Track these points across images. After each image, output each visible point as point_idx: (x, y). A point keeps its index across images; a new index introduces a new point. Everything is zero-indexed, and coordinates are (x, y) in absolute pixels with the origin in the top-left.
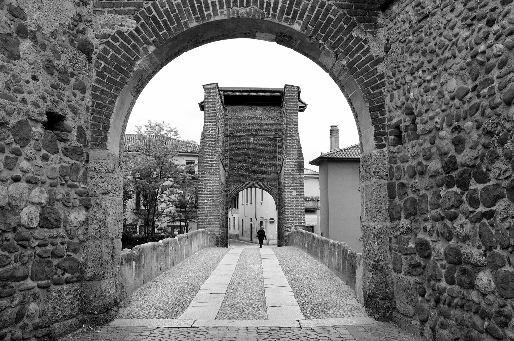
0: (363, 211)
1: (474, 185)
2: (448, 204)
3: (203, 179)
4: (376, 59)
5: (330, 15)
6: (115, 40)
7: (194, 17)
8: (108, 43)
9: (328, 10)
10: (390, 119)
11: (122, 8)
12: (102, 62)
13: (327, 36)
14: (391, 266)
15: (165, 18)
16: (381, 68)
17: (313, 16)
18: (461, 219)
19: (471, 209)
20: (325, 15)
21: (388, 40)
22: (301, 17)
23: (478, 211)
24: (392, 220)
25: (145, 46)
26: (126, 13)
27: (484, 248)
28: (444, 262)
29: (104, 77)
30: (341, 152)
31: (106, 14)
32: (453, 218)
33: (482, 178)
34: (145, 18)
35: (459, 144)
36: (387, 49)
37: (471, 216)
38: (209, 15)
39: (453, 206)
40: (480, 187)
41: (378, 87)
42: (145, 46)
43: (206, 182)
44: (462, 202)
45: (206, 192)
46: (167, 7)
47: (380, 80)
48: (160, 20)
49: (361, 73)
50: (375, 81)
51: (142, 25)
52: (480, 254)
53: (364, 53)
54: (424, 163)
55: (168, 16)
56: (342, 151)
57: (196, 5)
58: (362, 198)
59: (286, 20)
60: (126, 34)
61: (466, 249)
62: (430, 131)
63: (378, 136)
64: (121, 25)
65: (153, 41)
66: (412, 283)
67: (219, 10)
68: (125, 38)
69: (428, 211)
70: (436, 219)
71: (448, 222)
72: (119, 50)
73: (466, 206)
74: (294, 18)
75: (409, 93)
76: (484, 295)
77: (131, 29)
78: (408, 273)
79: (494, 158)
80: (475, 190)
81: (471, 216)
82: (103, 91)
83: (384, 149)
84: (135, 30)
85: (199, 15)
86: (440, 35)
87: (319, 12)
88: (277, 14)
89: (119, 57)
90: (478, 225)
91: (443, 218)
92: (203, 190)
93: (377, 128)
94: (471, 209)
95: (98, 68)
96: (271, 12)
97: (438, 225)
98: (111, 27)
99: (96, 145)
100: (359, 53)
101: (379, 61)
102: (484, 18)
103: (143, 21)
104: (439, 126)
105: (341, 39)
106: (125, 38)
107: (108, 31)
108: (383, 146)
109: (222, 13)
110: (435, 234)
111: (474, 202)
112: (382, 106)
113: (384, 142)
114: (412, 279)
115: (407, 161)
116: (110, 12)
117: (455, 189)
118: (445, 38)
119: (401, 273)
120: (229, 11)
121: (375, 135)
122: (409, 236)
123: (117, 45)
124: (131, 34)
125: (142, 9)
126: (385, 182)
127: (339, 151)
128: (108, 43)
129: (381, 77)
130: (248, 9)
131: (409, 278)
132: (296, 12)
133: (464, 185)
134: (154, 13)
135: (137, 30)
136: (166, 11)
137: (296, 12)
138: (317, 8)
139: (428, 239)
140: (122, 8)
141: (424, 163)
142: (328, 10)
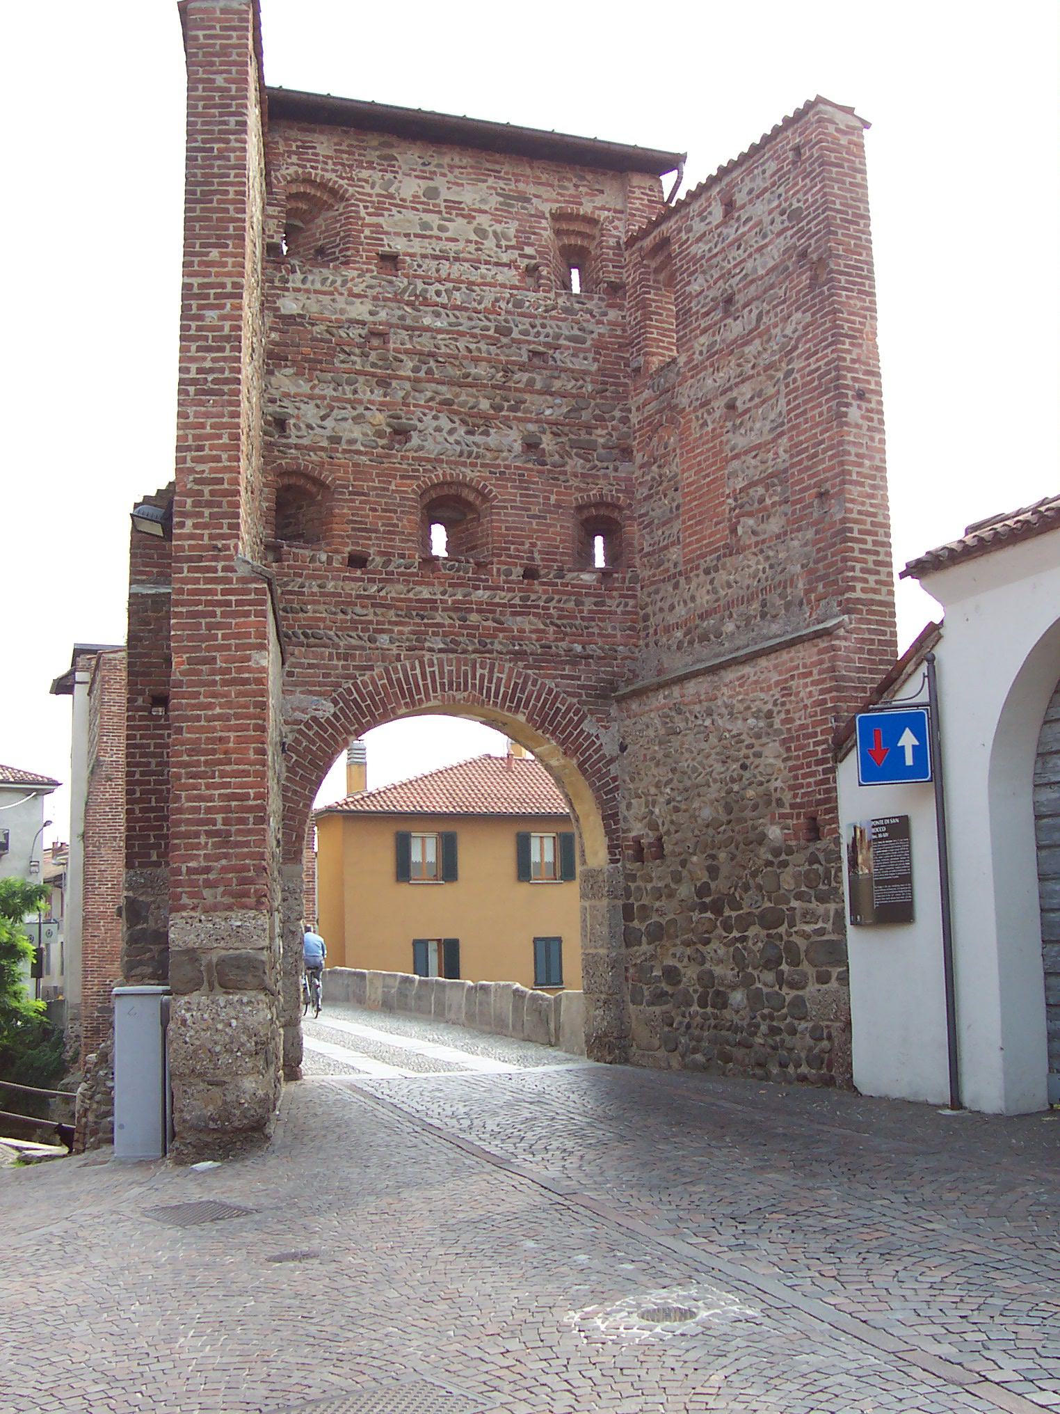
0: (585, 936)
1: (727, 912)
2: (701, 929)
3: (97, 861)
4: (609, 758)
5: (558, 705)
6: (309, 727)
7: (402, 702)
8: (300, 731)
9: (556, 698)
10: (628, 830)
11: (317, 688)
12: (293, 755)
13: (556, 729)
14: (628, 998)
15: (369, 702)
16: (614, 769)
17: (539, 705)
18: (714, 945)
19: (727, 935)
20: (553, 704)
21: (623, 738)
22: (526, 707)
23: (731, 936)
24: (628, 945)
25: (344, 736)
26: (320, 694)
27: (737, 970)
28: (697, 987)
29: (296, 774)
30: (372, 798)
31: (298, 695)
32: (707, 942)
33: (736, 906)
34: (346, 702)
35: (713, 871)
36: (623, 748)
37: (725, 941)
38: (420, 700)
39: (707, 932)
40: (734, 914)
41: (611, 791)
42: (344, 736)
43: (103, 868)
44: (716, 927)
45: (103, 888)
46: (371, 688)
47: (614, 782)
48: (363, 705)
49: (594, 774)
50: (607, 784)
51: (341, 709)
52: (734, 975)
53: (596, 752)
54: (673, 886)
55: (372, 699)
56: (374, 796)
57: (405, 687)
58: (584, 920)
59: (510, 709)
60: (322, 721)
61: (718, 970)
62: (680, 854)
63: (611, 848)
64: (315, 710)
65: (355, 731)
66: (657, 1013)
67: (432, 694)
68: (320, 725)
69: (677, 937)
70: (687, 944)
71: (699, 946)
72: (313, 740)
73: (720, 931)
74: (518, 706)
75: (654, 807)
76: (737, 1012)
77: (327, 715)
78: (650, 1004)
79: (746, 888)
80: (730, 917)
81: (725, 941)
82: (295, 792)
83: (619, 865)
84: (333, 716)
85: (408, 700)
86: (693, 759)
87: (546, 700)
88: (499, 701)
89: (314, 749)
90: (732, 949)
91: (695, 943)
92: (97, 884)
93: (611, 839)
94: (727, 935)
95: (289, 761)
96: (492, 699)
97: (688, 951)
98: (304, 711)
99: (289, 859)
100: (591, 751)
101: (612, 761)
102: (738, 761)
103: (342, 704)
104: (691, 851)
105: (571, 734)
106: (320, 725)
107: (299, 715)
108: (618, 861)
109: (435, 697)
110: (686, 960)
111: (728, 928)
112: (616, 814)
113: (618, 857)
114: (657, 1009)
115: (651, 881)
116: (302, 692)
117: (709, 914)
118: (698, 763)
119: (641, 1004)
120: (443, 696)
121: (609, 847)
122: (653, 963)
123: (311, 733)
124: (328, 720)
125: (341, 690)
126: (620, 903)
127: (368, 797)
128: (300, 731)
129: (615, 779)
130: (466, 693)
131: (654, 1008)
132: (520, 699)
133: (718, 911)
134: (356, 695)
135: (335, 715)
136: (369, 693)
137: (520, 699)
138: (544, 695)
139: (678, 965)
140: (317, 688)
141: (673, 886)
142: (556, 698)
